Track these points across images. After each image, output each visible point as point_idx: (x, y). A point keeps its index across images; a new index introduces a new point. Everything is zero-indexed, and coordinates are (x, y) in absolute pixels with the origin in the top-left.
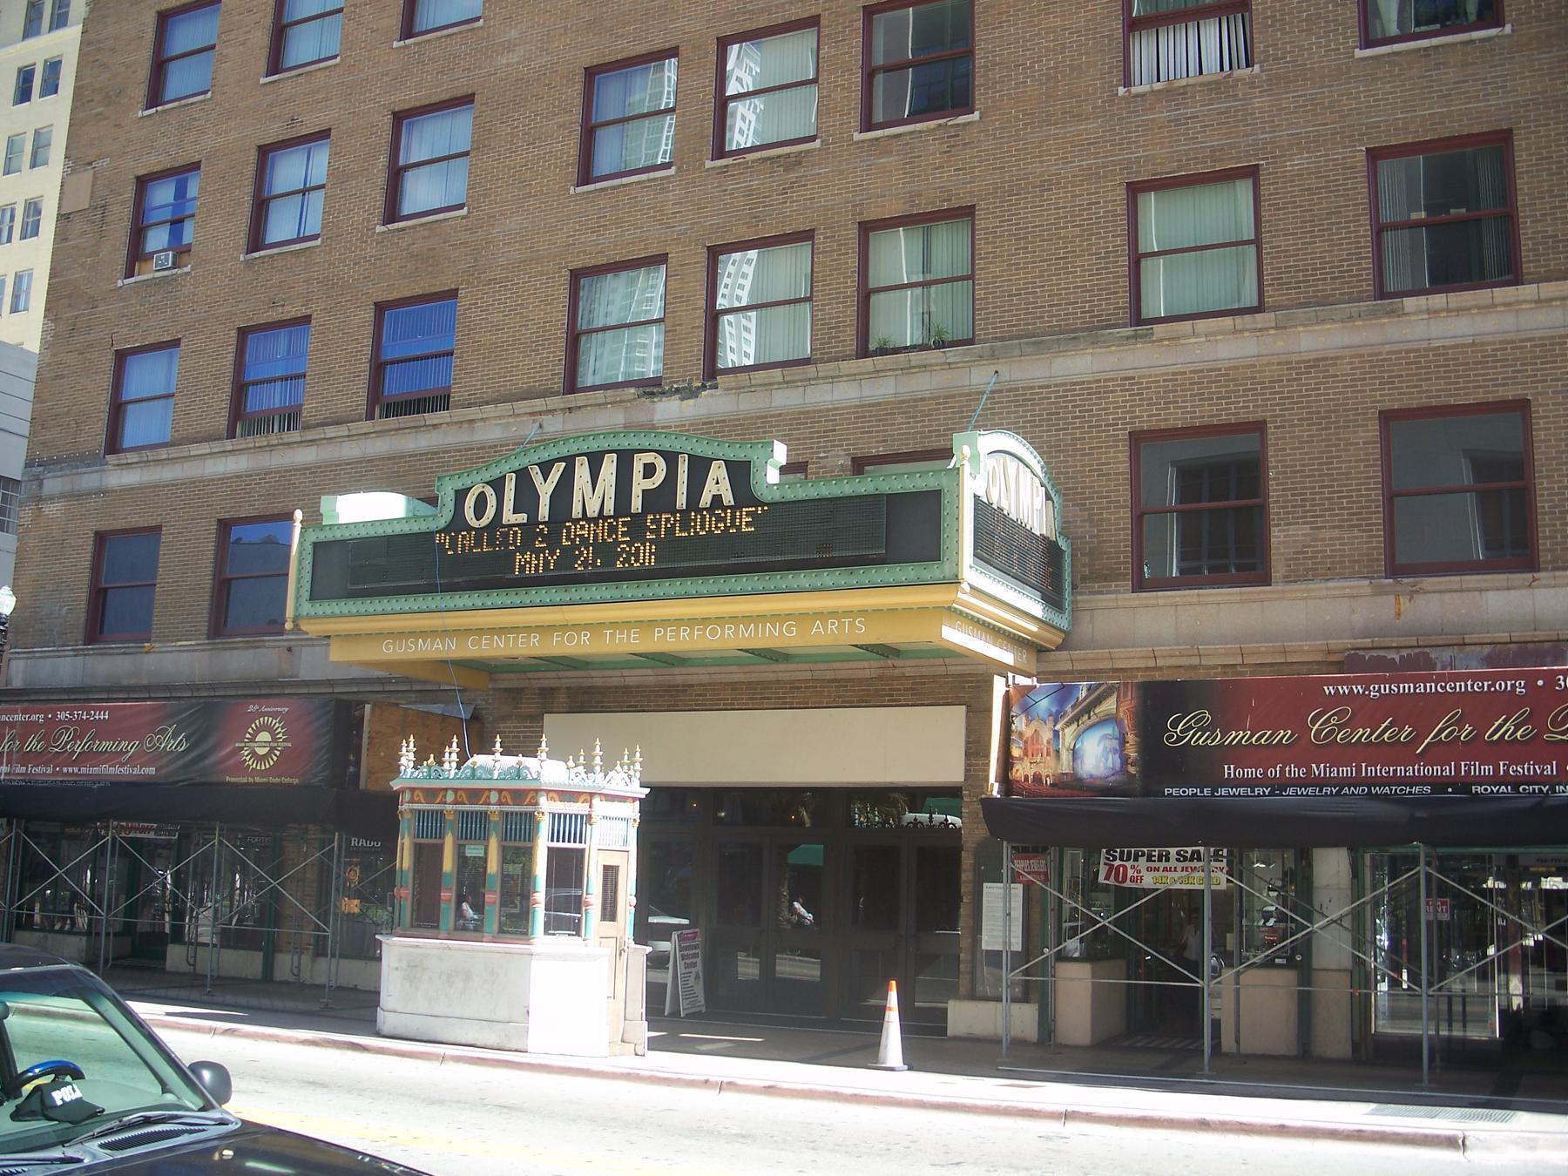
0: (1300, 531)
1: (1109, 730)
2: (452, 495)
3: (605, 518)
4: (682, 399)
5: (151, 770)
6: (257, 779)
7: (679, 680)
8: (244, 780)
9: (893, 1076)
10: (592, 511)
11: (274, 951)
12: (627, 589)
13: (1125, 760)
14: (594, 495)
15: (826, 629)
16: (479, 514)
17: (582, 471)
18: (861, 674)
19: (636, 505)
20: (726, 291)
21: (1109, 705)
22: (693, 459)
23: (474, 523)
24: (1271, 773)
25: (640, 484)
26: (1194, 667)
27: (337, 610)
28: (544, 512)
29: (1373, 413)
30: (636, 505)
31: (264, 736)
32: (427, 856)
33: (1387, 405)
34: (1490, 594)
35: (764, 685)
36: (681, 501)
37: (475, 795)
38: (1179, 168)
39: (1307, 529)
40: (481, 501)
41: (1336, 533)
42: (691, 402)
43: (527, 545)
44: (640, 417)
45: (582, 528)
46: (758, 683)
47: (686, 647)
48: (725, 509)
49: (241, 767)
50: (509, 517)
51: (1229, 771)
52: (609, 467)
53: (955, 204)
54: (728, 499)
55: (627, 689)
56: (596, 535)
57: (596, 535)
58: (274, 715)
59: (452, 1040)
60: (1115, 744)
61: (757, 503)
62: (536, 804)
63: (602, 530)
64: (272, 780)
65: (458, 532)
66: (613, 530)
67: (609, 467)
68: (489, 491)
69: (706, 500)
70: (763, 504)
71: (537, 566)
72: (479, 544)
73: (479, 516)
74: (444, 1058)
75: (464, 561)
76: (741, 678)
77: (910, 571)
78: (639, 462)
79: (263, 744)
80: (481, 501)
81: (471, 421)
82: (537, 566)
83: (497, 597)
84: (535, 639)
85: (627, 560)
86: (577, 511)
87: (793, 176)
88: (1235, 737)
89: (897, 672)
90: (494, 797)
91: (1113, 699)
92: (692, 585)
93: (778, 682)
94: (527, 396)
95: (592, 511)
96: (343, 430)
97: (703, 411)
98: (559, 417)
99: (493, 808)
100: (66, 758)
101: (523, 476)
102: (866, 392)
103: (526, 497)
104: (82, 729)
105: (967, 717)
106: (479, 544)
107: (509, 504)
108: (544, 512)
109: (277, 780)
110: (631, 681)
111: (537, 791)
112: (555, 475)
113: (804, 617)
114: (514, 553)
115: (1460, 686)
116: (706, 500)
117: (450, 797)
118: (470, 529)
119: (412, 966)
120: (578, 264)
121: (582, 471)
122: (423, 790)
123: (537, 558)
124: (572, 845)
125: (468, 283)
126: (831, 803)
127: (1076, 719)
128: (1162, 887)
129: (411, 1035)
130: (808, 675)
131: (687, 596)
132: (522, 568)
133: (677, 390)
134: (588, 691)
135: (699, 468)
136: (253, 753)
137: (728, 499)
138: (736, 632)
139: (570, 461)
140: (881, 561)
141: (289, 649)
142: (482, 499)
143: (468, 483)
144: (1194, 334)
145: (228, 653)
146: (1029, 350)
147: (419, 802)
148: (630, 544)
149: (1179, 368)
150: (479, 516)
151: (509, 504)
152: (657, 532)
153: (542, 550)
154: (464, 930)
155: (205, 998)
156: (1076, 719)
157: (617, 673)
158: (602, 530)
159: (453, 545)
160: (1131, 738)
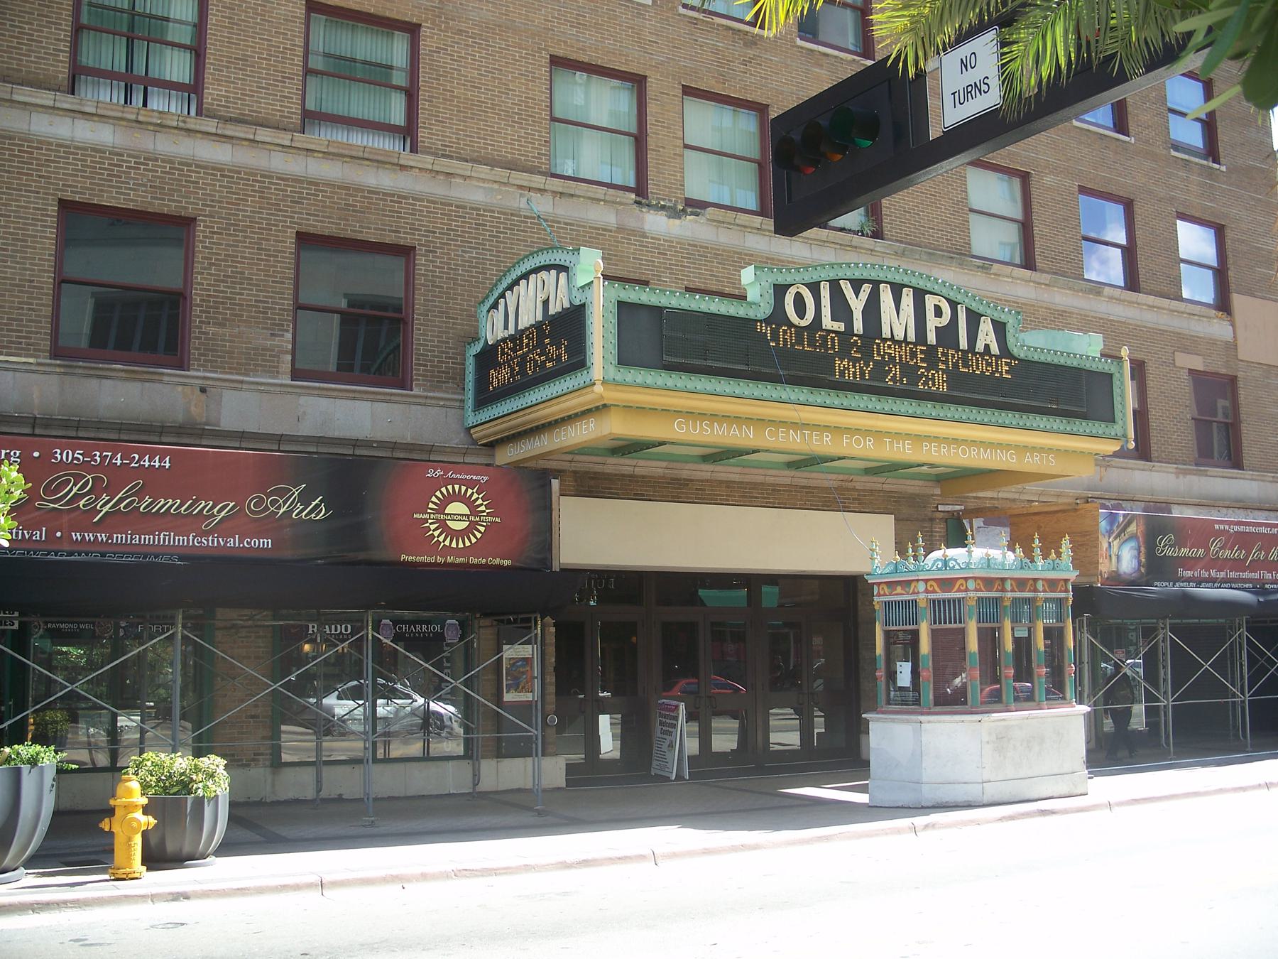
1: (1133, 544)
3: (908, 343)
4: (669, 217)
5: (267, 543)
6: (450, 559)
8: (431, 559)
10: (899, 335)
12: (928, 408)
13: (1140, 562)
14: (897, 321)
16: (801, 312)
17: (886, 296)
18: (826, 484)
19: (932, 338)
21: (1133, 528)
23: (804, 323)
24: (1197, 574)
25: (932, 323)
26: (1014, 500)
27: (650, 380)
28: (858, 326)
30: (932, 338)
31: (457, 508)
32: (990, 639)
34: (1137, 472)
35: (754, 485)
36: (963, 344)
37: (946, 584)
42: (677, 222)
43: (844, 353)
44: (631, 223)
45: (889, 347)
46: (748, 483)
47: (593, 436)
48: (991, 356)
49: (427, 543)
50: (827, 322)
51: (1181, 572)
54: (995, 349)
56: (901, 356)
57: (901, 356)
58: (470, 484)
59: (1036, 796)
60: (1136, 552)
61: (1013, 357)
63: (905, 353)
64: (474, 560)
65: (779, 326)
66: (913, 355)
70: (1016, 359)
71: (854, 373)
72: (800, 341)
73: (801, 315)
74: (1065, 812)
75: (787, 356)
76: (736, 478)
78: (930, 301)
79: (457, 517)
82: (854, 373)
83: (821, 396)
84: (827, 438)
85: (925, 383)
86: (886, 333)
87: (751, 52)
88: (1184, 551)
89: (850, 485)
90: (1040, 586)
91: (1134, 525)
92: (973, 413)
94: (512, 166)
97: (688, 234)
98: (549, 198)
99: (971, 594)
100: (85, 520)
101: (835, 285)
102: (815, 256)
103: (841, 309)
104: (111, 480)
106: (800, 341)
108: (858, 326)
109: (482, 561)
112: (864, 295)
113: (1022, 449)
114: (832, 358)
115: (1261, 530)
118: (791, 325)
119: (1000, 738)
120: (560, 53)
121: (886, 296)
122: (984, 579)
123: (854, 367)
124: (953, 626)
126: (682, 586)
127: (1118, 536)
128: (516, 646)
129: (1005, 799)
130: (788, 481)
131: (968, 421)
132: (842, 373)
133: (663, 207)
134: (596, 476)
135: (974, 319)
136: (443, 525)
137: (995, 349)
138: (979, 453)
139: (876, 284)
140: (1084, 417)
141: (203, 390)
142: (799, 300)
143: (789, 280)
145: (94, 382)
146: (924, 257)
147: (934, 592)
148: (928, 370)
149: (999, 295)
150: (801, 315)
152: (946, 362)
153: (858, 360)
154: (1026, 699)
155: (362, 831)
156: (1118, 536)
157: (761, 471)
158: (905, 353)
159: (775, 337)
160: (1142, 549)
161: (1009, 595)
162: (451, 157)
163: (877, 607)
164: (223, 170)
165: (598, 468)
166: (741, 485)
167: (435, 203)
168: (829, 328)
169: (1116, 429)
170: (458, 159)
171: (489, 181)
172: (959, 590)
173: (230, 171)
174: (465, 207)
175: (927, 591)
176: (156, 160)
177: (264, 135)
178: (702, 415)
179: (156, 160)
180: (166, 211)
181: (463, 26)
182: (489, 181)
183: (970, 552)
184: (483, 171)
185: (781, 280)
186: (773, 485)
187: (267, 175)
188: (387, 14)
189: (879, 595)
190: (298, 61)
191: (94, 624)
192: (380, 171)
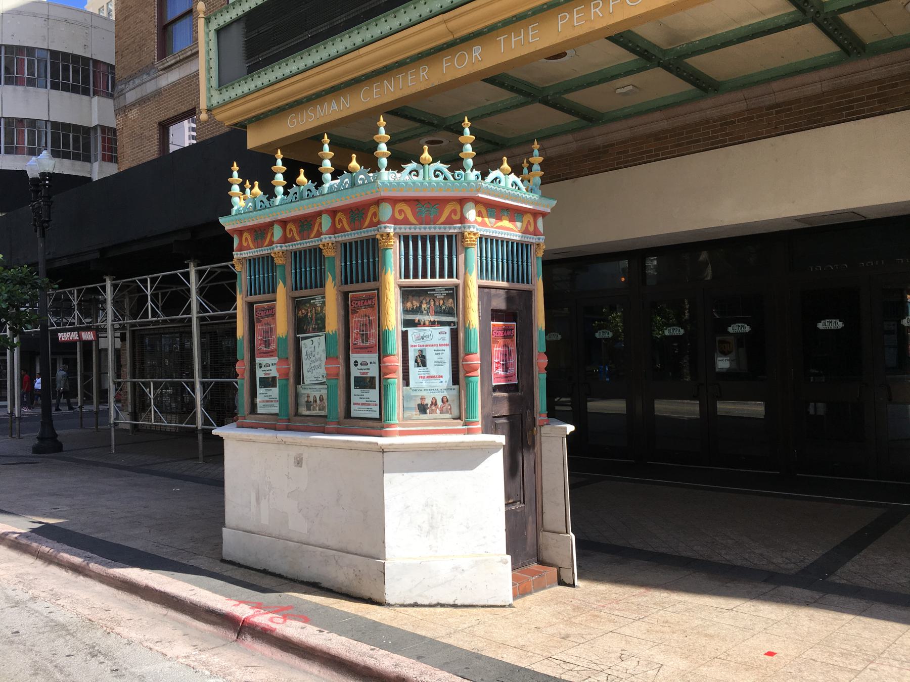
7: (599, 141)
62: (463, 220)
76: (664, 125)
130: (743, 106)
161: (277, 248)
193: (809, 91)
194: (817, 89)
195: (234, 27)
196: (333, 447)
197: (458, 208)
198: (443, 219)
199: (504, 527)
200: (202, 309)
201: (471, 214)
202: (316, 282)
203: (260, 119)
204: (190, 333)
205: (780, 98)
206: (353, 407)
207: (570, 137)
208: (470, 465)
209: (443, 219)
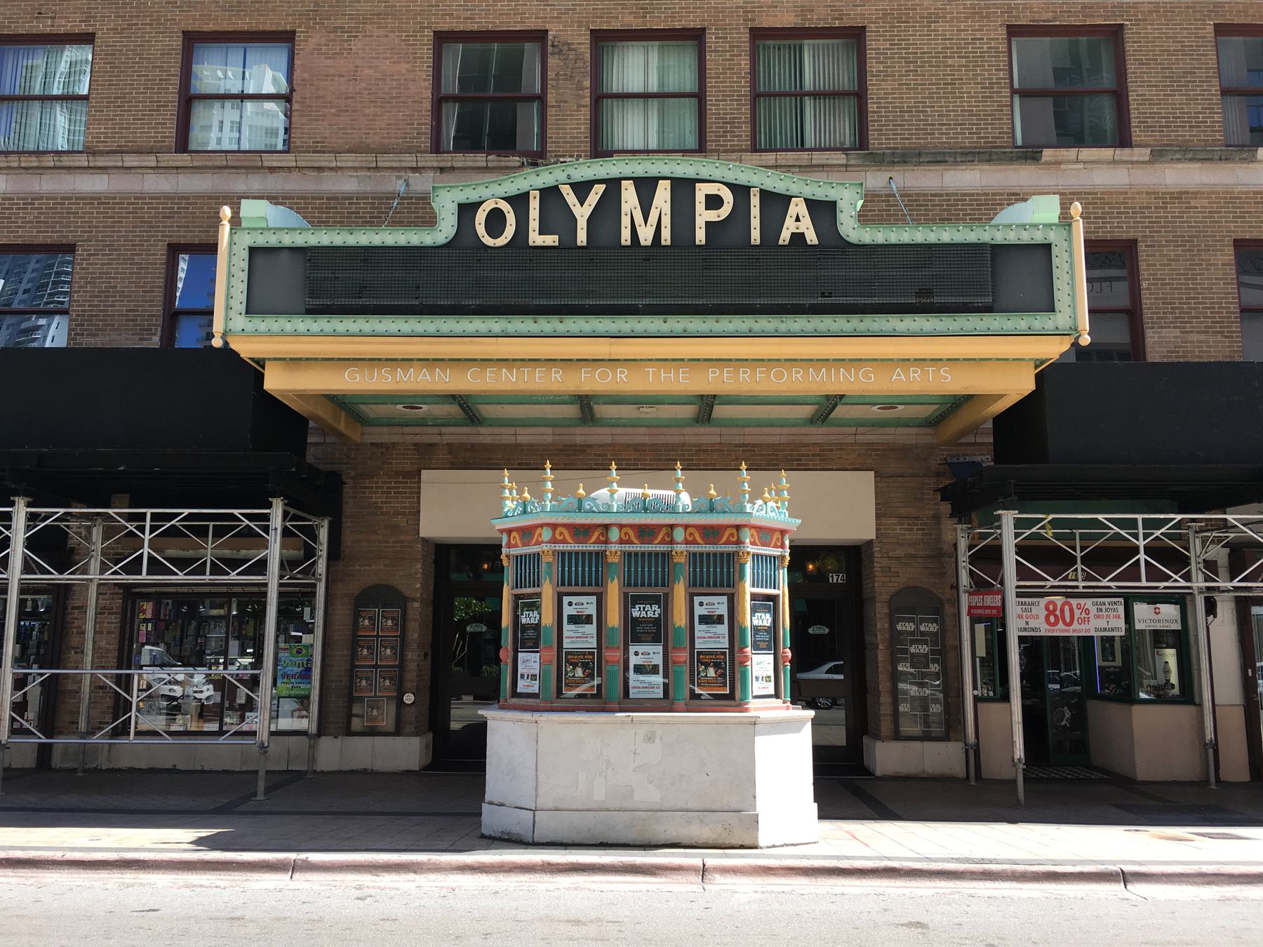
0: (1172, 334)
2: (453, 208)
7: (579, 440)
9: (759, 809)
11: (865, 731)
15: (908, 377)
17: (629, 196)
20: (554, 83)
22: (764, 194)
23: (488, 241)
25: (703, 216)
29: (1229, 241)
33: (1240, 235)
38: (1054, 19)
39: (1177, 332)
40: (496, 219)
41: (1203, 337)
50: (536, 239)
52: (663, 195)
53: (846, 23)
55: (517, 447)
62: (739, 542)
67: (663, 195)
68: (505, 207)
69: (785, 237)
76: (646, 440)
77: (1021, 322)
78: (702, 191)
80: (496, 219)
81: (320, 169)
90: (679, 535)
93: (684, 445)
95: (646, 236)
96: (150, 161)
99: (545, 547)
105: (876, 482)
107: (534, 224)
110: (522, 439)
111: (738, 527)
116: (785, 237)
117: (614, 534)
120: (445, 27)
121: (629, 196)
125: (308, 27)
130: (717, 439)
140: (988, 309)
144: (1077, 161)
147: (564, 542)
151: (534, 224)
157: (512, 430)
161: (614, 548)
162: (324, 152)
163: (505, 563)
164: (99, 198)
165: (473, 440)
166: (655, 448)
167: (304, 198)
168: (538, 244)
169: (246, 240)
170: (314, 152)
171: (362, 168)
172: (728, 542)
173: (106, 198)
174: (337, 199)
175: (554, 541)
176: (42, 198)
177: (130, 160)
178: (392, 361)
179: (42, 198)
180: (49, 241)
181: (338, 23)
182: (362, 168)
183: (613, 492)
184: (348, 160)
185: (471, 195)
186: (694, 445)
187: (140, 197)
188: (261, 28)
189: (509, 546)
190: (296, 106)
191: (1181, 599)
192: (250, 176)
193: (770, 440)
194: (776, 440)
195: (285, 256)
196: (696, 723)
197: (734, 531)
198: (724, 539)
199: (811, 781)
200: (28, 567)
201: (747, 536)
202: (643, 579)
203: (295, 362)
204: (280, 612)
205: (748, 440)
206: (631, 691)
207: (549, 430)
208: (798, 730)
209: (724, 539)
